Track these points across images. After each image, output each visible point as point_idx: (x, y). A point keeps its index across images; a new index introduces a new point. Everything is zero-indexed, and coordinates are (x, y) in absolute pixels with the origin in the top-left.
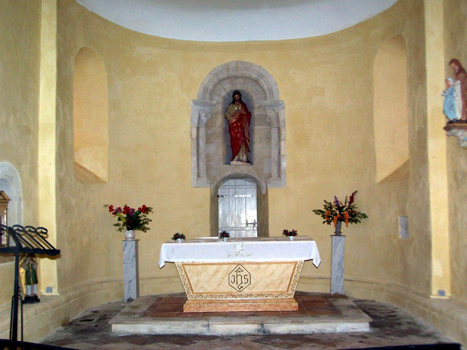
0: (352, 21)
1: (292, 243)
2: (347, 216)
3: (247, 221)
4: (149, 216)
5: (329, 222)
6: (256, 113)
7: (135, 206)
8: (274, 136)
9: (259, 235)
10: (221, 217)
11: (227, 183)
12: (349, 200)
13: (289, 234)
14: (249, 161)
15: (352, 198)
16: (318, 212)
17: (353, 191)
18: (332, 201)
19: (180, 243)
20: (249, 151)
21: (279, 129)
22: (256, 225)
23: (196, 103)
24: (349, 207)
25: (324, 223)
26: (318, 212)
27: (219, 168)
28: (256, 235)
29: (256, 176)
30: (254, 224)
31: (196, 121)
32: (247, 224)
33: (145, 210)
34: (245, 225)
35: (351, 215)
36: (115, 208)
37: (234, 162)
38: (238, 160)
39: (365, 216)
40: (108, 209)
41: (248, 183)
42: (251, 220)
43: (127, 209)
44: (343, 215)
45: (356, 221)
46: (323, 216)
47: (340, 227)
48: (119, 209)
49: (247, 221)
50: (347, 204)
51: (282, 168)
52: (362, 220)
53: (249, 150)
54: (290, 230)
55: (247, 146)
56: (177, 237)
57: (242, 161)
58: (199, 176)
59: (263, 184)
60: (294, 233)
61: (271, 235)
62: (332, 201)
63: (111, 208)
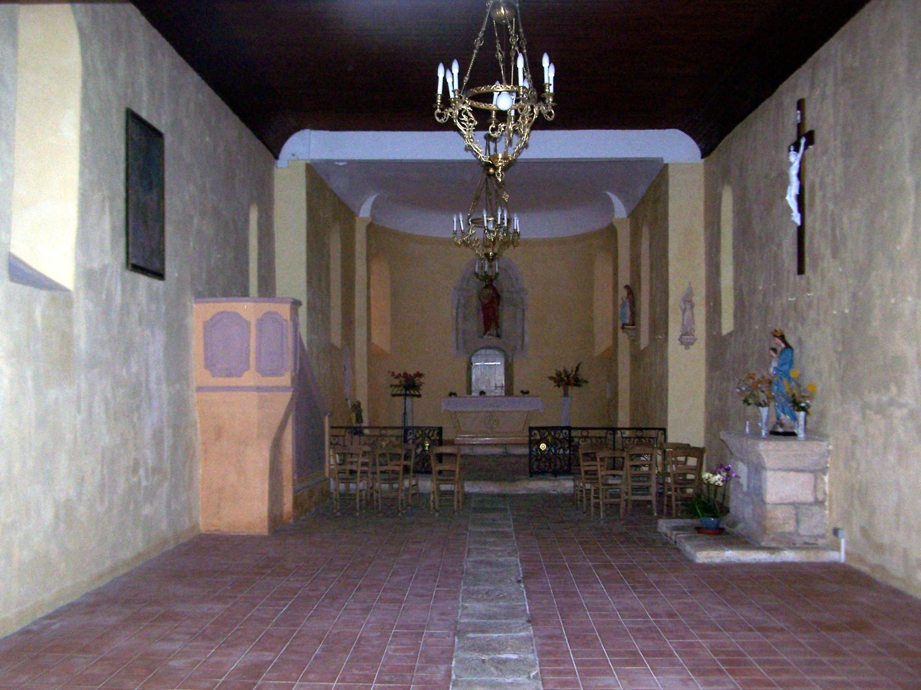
0: (579, 231)
1: (527, 399)
2: (573, 382)
3: (496, 384)
4: (422, 380)
5: (559, 386)
6: (505, 295)
7: (411, 372)
8: (519, 316)
9: (506, 394)
10: (77, 289)
11: (479, 352)
12: (574, 369)
13: (525, 393)
14: (498, 336)
15: (577, 368)
16: (551, 378)
17: (578, 362)
18: (562, 370)
19: (453, 398)
20: (498, 327)
21: (523, 311)
22: (504, 388)
23: (455, 289)
24: (576, 375)
25: (555, 386)
26: (551, 378)
27: (295, 158)
28: (504, 394)
29: (504, 348)
30: (502, 387)
31: (456, 302)
32: (496, 387)
33: (419, 375)
34: (494, 388)
35: (575, 381)
36: (396, 374)
37: (486, 337)
38: (489, 335)
39: (586, 382)
40: (391, 374)
41: (497, 352)
42: (499, 384)
43: (405, 375)
44: (569, 381)
45: (579, 386)
46: (555, 382)
47: (567, 390)
48: (400, 374)
49: (496, 384)
50: (574, 373)
51: (525, 342)
52: (584, 385)
53: (497, 326)
54: (525, 391)
55: (497, 323)
56: (451, 394)
57: (493, 335)
58: (458, 348)
59: (510, 354)
60: (527, 393)
61: (515, 394)
62: (562, 370)
63: (393, 374)
